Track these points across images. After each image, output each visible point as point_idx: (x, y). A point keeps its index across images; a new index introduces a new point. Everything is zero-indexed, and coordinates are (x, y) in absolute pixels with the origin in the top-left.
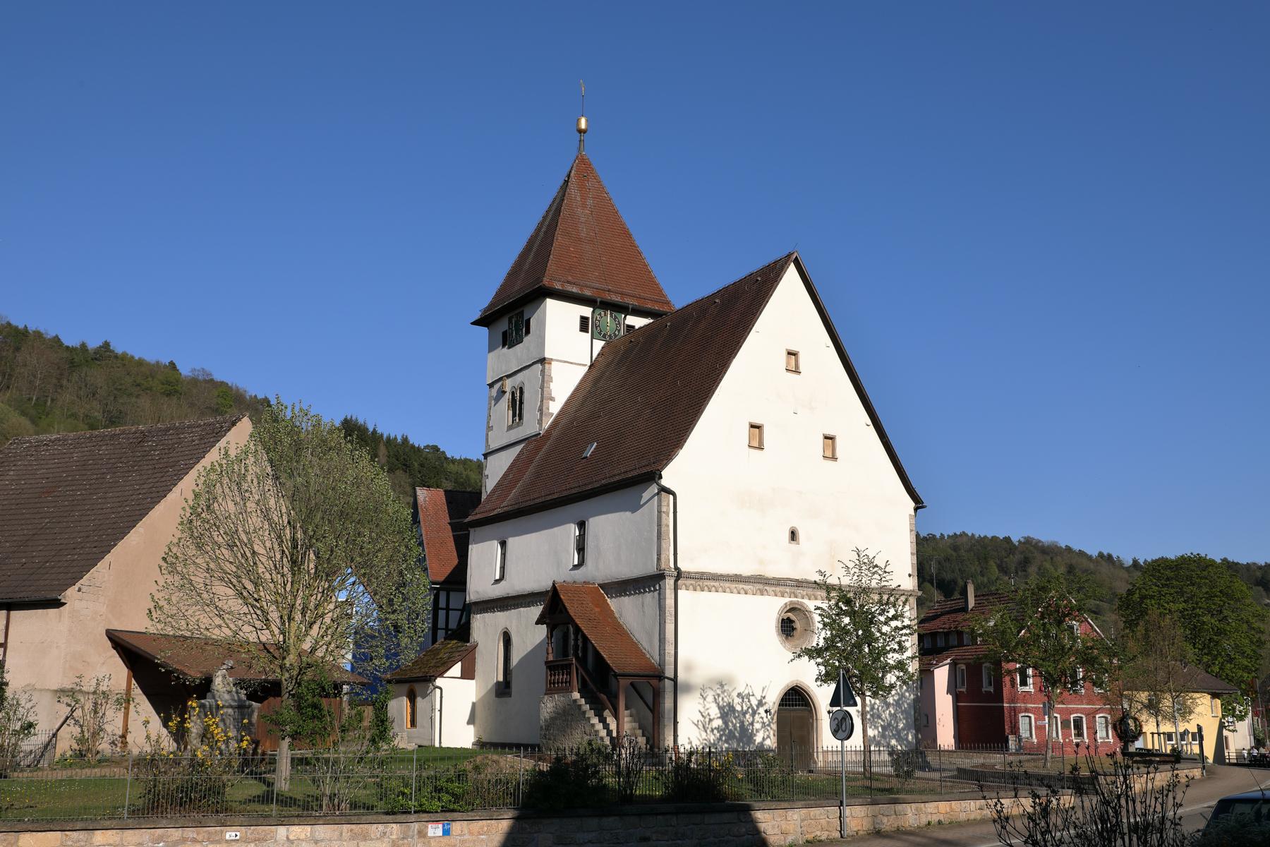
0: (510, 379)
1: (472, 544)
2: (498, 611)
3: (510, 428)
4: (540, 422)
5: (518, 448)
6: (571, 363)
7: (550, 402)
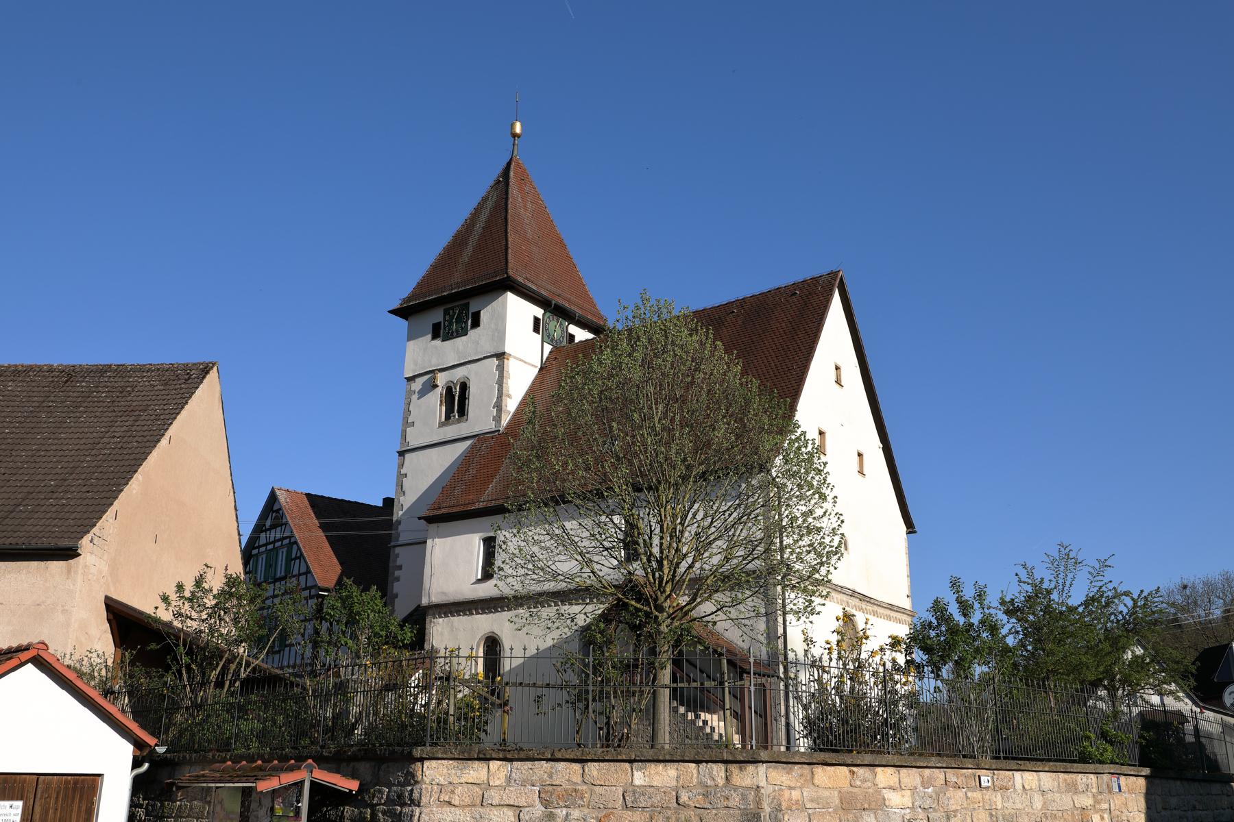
0: (443, 373)
1: (433, 538)
2: (479, 613)
3: (442, 425)
4: (498, 419)
5: (463, 447)
6: (526, 362)
7: (508, 399)
